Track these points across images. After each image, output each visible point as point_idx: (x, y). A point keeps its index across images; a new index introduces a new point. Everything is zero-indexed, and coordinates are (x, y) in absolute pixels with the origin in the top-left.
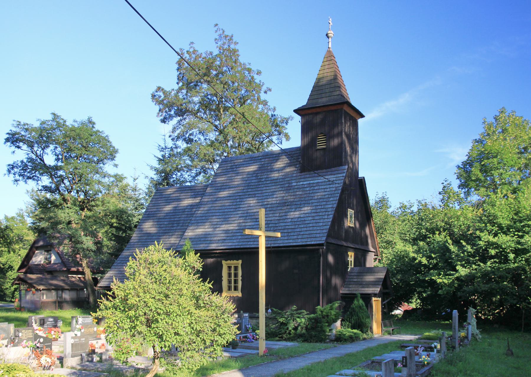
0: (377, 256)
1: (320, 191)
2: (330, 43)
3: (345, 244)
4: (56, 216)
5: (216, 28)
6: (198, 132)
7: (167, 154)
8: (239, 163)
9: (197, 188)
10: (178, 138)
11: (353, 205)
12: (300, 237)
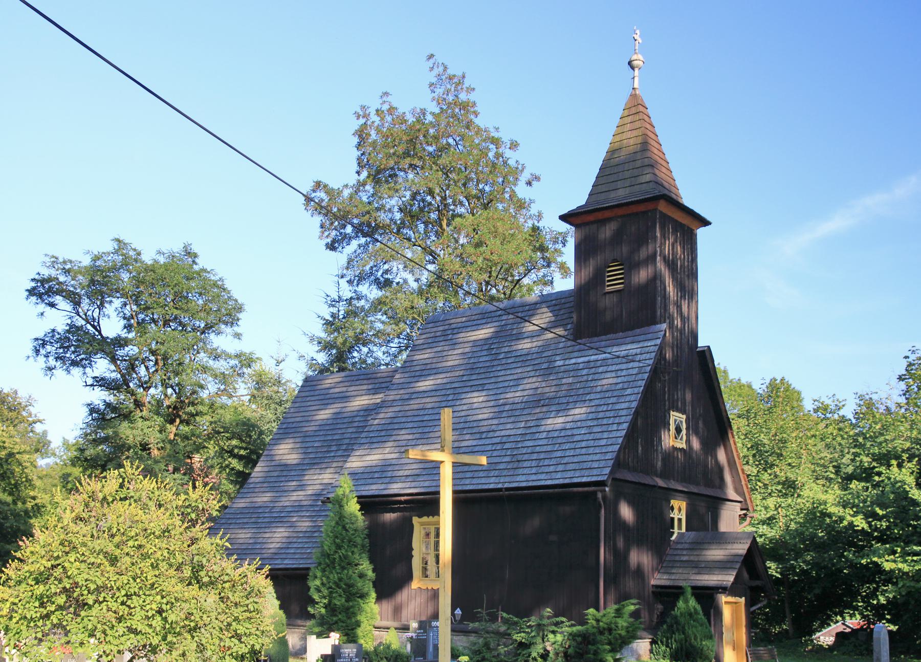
0: (747, 509)
1: (609, 375)
2: (636, 80)
3: (661, 483)
4: (116, 434)
6: (401, 267)
7: (342, 312)
8: (460, 325)
9: (379, 375)
10: (361, 278)
12: (560, 468)
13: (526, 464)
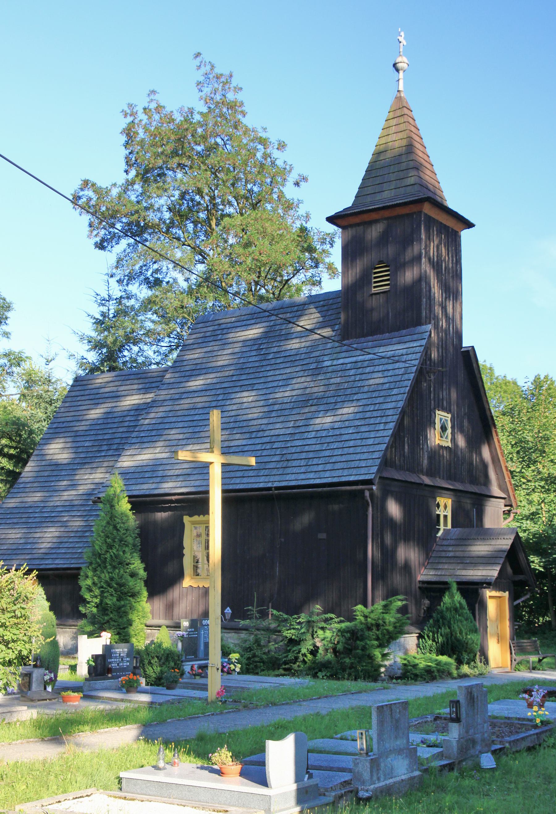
0: (511, 506)
1: (375, 375)
2: (401, 82)
3: (427, 480)
5: (197, 62)
7: (112, 311)
10: (131, 277)
11: (449, 403)
13: (295, 463)
